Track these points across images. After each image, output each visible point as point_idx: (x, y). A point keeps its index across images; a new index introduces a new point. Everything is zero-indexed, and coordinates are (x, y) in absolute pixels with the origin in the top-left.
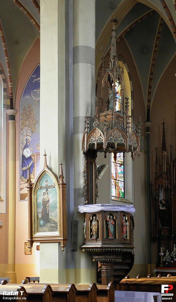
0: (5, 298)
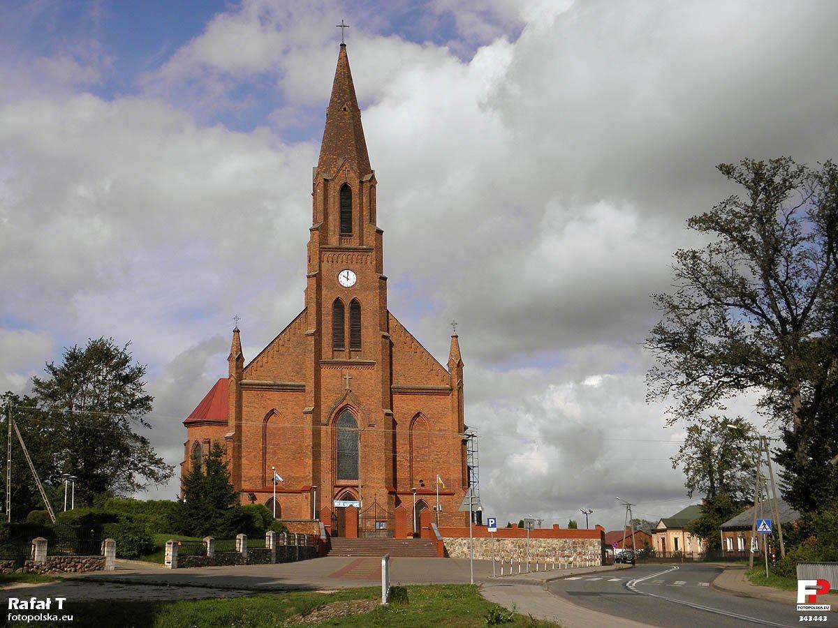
0: (15, 618)
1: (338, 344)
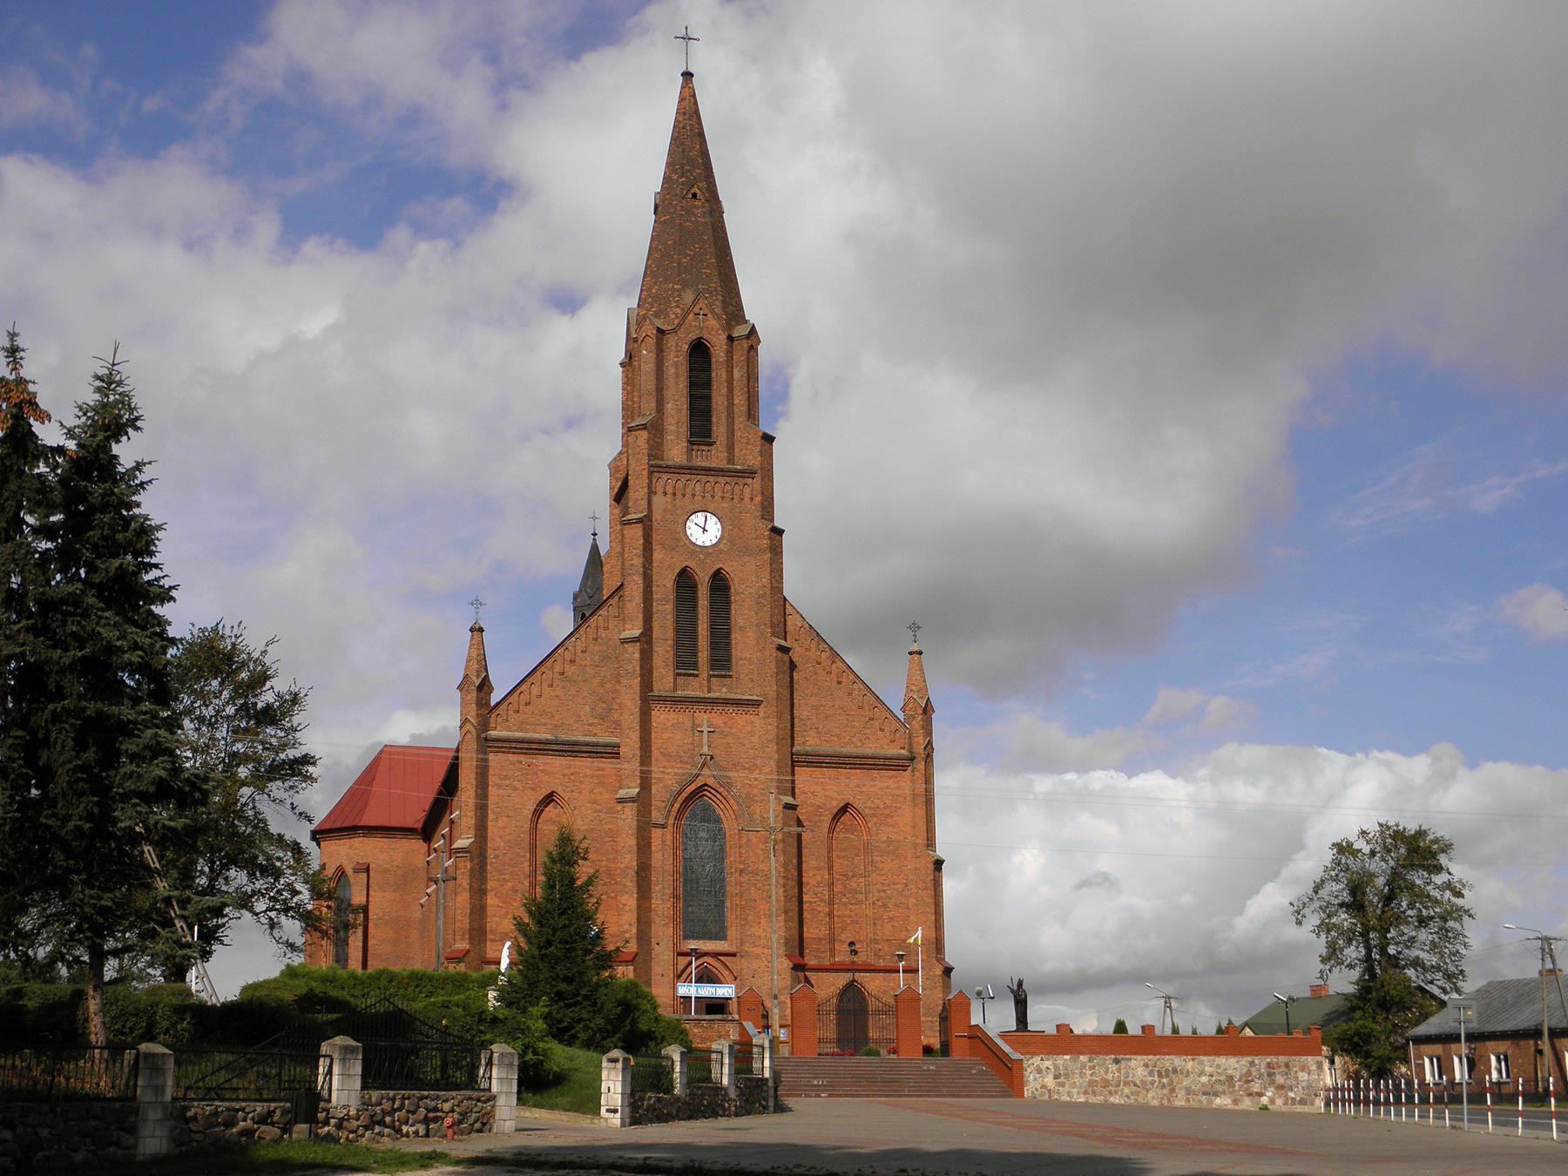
1: (685, 662)
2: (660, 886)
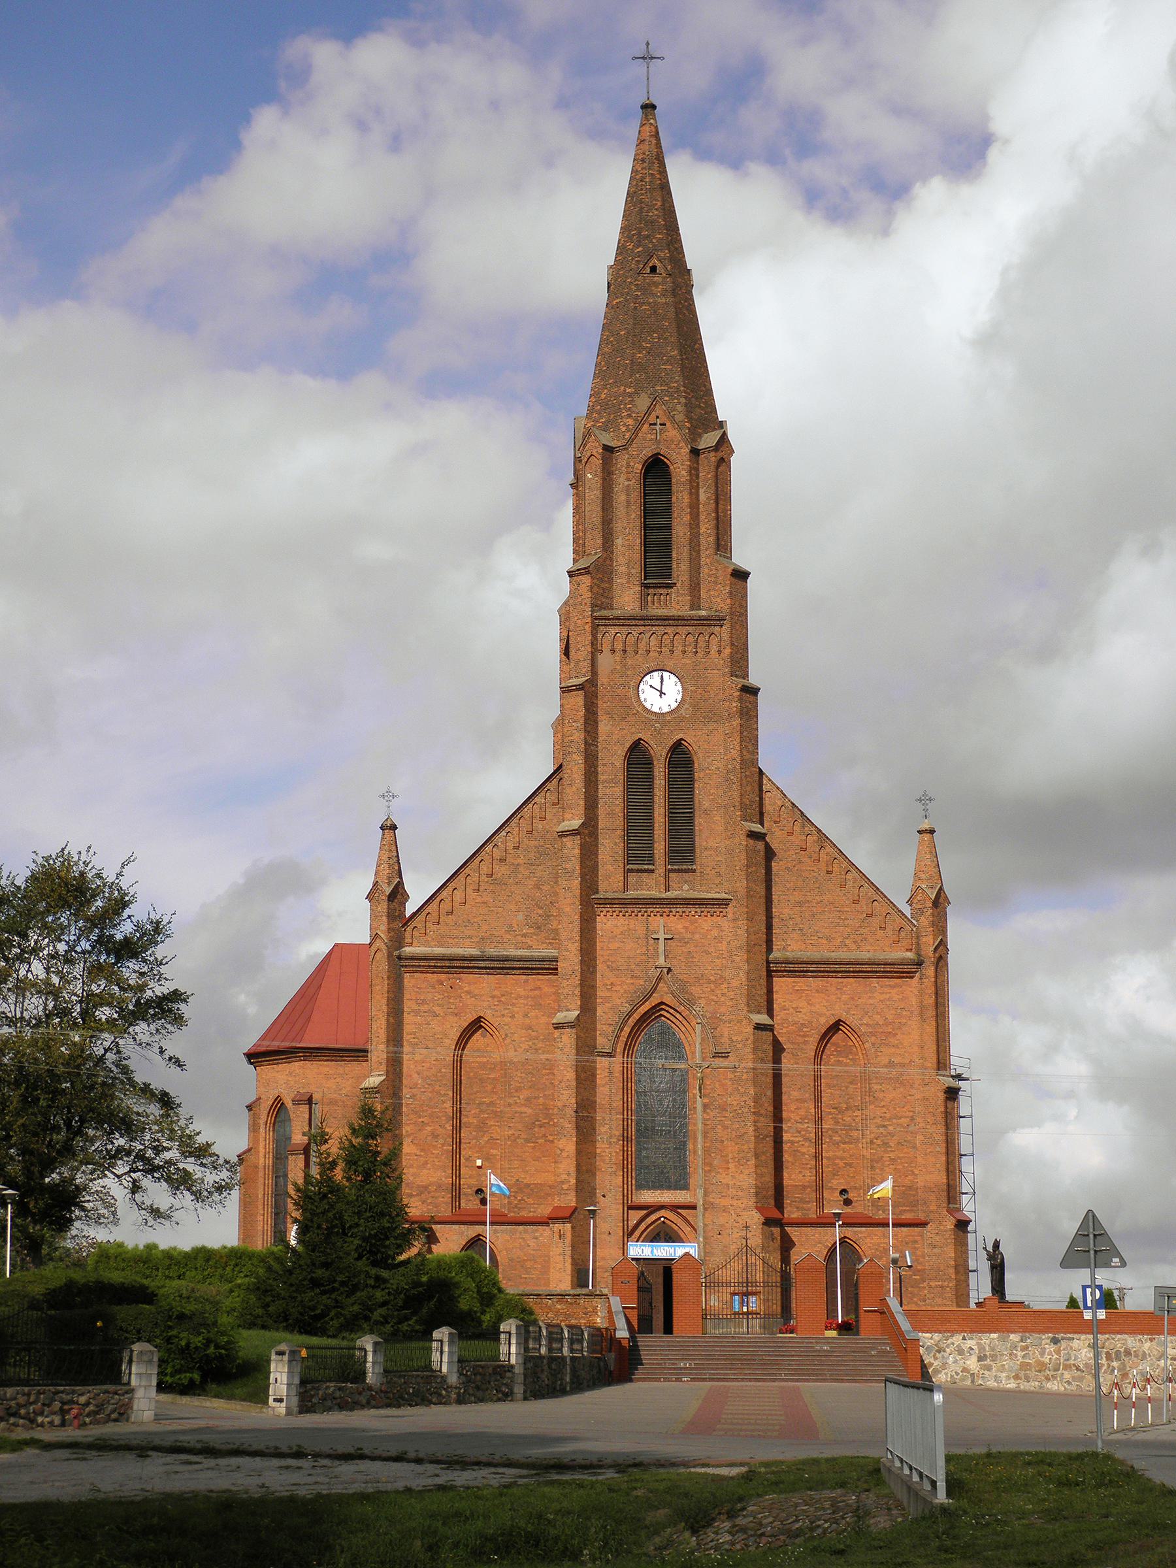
2: (607, 1126)
